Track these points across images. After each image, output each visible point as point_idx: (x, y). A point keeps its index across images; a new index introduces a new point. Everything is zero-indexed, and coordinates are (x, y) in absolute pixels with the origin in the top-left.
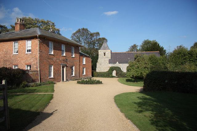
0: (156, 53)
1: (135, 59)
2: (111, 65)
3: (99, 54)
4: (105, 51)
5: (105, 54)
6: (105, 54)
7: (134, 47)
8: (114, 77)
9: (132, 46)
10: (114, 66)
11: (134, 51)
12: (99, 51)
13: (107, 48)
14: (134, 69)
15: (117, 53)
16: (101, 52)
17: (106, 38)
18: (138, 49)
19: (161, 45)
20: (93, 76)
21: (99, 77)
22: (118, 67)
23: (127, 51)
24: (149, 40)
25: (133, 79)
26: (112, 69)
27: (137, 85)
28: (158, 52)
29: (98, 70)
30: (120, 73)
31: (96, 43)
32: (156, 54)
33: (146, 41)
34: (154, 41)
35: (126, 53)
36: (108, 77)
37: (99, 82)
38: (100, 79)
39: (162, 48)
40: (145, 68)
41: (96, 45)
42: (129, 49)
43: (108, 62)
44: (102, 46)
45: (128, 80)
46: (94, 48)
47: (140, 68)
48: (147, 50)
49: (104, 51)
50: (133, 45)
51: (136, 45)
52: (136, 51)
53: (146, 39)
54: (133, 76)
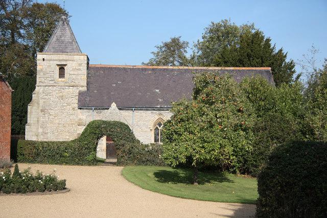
0: (261, 72)
1: (197, 92)
2: (89, 116)
3: (39, 68)
4: (63, 57)
5: (62, 68)
6: (62, 68)
7: (173, 48)
8: (102, 162)
9: (166, 45)
10: (98, 118)
11: (172, 62)
12: (40, 56)
13: (71, 46)
14: (191, 133)
15: (110, 69)
16: (46, 63)
17: (67, 8)
18: (188, 56)
19: (277, 45)
20: (14, 157)
21: (41, 162)
22: (122, 124)
23: (147, 61)
24: (231, 23)
25: (182, 173)
26: (95, 131)
27: (207, 194)
28: (267, 72)
29: (32, 134)
30: (128, 146)
31: (21, 23)
32: (259, 74)
33: (219, 26)
34: (247, 28)
35: (145, 70)
36: (78, 164)
37: (54, 186)
38: (60, 172)
39: (281, 56)
40: (236, 128)
41: (22, 31)
42: (152, 56)
43: (75, 102)
44: (53, 39)
45: (163, 177)
46: (14, 42)
47: (217, 128)
48: (224, 61)
49: (61, 58)
50: (169, 40)
51: (181, 40)
52: (181, 64)
53: (217, 21)
54: (190, 159)
